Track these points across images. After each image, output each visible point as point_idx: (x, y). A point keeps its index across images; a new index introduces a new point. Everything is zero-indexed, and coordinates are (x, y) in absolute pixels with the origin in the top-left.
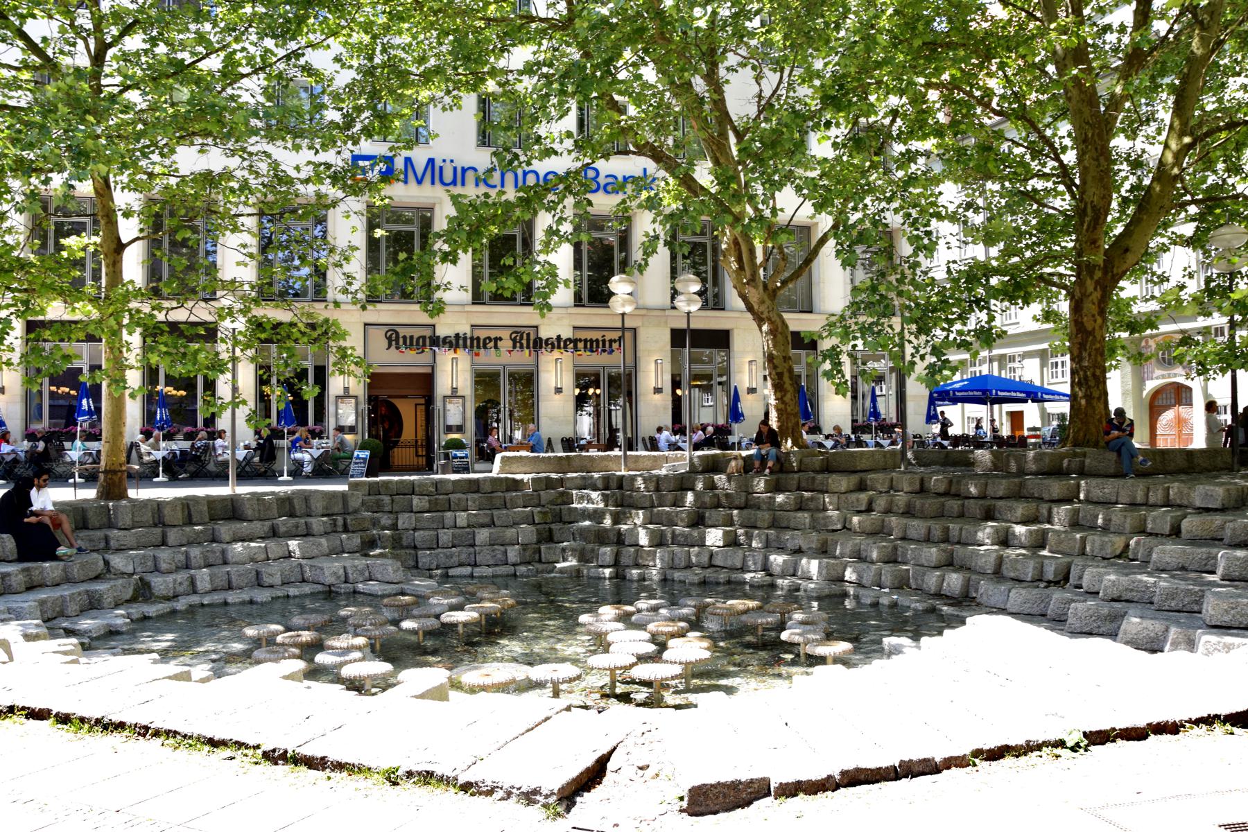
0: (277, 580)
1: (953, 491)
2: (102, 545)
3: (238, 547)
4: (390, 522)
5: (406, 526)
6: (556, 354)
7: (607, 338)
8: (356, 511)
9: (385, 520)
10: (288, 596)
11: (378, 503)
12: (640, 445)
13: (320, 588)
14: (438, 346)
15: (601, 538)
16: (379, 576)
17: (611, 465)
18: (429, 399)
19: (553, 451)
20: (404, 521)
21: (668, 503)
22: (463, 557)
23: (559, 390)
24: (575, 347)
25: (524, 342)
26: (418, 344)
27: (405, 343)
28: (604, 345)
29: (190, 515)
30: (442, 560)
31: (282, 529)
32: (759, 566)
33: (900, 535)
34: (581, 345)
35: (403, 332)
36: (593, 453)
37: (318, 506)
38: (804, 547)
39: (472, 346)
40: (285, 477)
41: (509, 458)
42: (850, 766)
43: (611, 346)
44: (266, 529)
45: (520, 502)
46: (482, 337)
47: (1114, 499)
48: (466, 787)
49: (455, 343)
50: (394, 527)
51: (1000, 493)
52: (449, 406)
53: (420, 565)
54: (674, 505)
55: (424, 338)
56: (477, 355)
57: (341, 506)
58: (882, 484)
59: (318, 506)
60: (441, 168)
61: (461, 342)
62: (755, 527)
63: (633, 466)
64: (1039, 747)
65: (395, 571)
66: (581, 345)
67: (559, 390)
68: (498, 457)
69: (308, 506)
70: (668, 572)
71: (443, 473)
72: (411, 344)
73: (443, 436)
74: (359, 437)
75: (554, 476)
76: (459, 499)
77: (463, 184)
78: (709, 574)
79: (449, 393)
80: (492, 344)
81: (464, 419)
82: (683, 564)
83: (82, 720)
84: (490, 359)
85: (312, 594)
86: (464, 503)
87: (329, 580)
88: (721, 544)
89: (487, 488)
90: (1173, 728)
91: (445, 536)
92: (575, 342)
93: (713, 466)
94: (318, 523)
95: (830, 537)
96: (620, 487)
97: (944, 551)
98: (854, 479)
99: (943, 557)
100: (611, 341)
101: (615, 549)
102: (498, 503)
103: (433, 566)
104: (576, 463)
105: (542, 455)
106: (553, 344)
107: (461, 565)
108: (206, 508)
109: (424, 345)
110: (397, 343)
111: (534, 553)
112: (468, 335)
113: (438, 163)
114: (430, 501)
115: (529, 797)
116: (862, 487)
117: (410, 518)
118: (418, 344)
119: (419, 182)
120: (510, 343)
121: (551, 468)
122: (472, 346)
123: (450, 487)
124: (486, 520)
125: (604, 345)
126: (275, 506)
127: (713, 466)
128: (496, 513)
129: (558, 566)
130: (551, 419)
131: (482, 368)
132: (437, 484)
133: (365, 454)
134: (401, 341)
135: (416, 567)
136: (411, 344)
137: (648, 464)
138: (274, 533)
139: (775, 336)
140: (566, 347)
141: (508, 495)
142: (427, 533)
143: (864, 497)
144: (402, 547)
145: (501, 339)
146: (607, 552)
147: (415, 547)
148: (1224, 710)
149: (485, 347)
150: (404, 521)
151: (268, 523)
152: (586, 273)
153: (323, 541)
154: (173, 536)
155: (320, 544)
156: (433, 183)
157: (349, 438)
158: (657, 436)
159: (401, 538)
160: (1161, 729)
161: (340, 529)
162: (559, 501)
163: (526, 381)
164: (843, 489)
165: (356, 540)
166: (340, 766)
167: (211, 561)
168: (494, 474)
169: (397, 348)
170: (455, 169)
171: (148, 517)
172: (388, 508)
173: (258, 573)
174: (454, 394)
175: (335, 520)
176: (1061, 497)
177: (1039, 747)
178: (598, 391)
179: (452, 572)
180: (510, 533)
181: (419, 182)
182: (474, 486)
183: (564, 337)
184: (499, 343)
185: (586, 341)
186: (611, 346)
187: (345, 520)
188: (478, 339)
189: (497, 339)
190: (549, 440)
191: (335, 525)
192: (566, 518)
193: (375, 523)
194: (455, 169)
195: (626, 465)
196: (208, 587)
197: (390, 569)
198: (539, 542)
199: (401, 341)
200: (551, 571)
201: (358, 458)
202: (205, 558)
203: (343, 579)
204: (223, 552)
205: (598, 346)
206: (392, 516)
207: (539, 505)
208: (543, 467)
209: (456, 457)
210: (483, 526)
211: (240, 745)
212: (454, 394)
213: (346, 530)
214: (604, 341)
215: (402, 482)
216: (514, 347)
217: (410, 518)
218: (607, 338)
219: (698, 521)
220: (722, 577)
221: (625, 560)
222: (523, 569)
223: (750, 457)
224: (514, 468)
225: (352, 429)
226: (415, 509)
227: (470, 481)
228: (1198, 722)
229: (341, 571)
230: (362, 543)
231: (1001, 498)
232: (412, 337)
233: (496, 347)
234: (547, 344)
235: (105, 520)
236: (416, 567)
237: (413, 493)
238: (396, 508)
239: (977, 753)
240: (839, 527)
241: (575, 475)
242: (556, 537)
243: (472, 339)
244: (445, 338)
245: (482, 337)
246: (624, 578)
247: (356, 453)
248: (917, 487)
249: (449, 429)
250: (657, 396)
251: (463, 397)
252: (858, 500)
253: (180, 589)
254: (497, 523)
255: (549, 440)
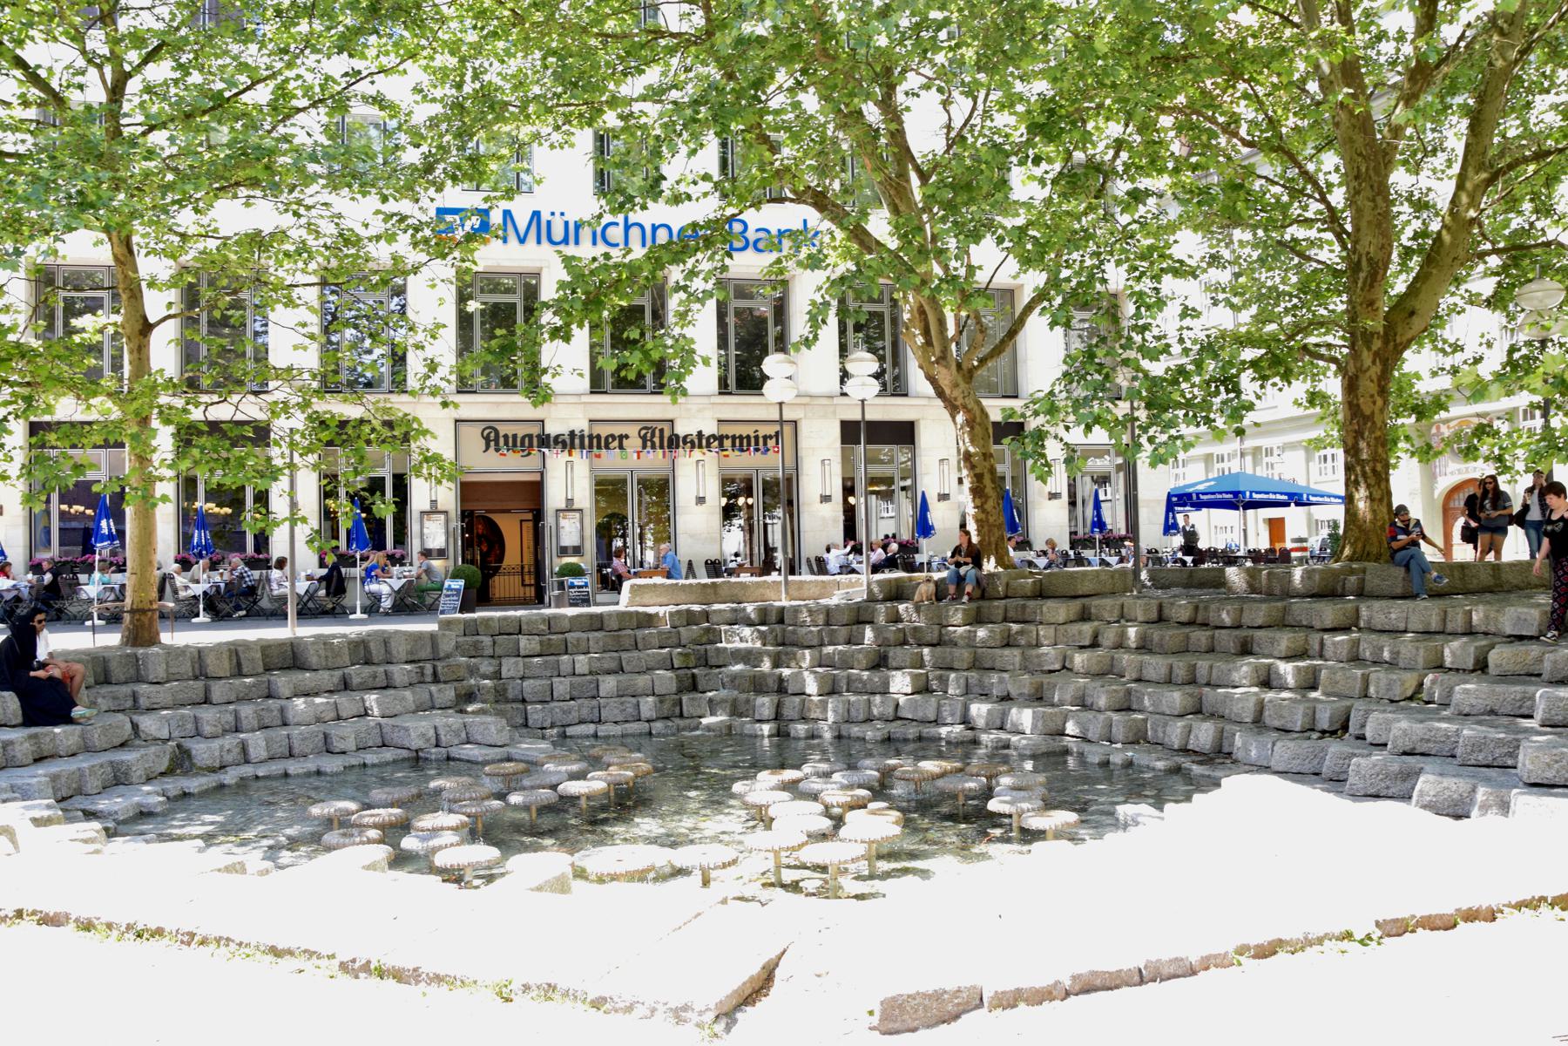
0: (350, 744)
1: (1200, 619)
2: (129, 704)
3: (300, 703)
4: (491, 669)
5: (512, 674)
6: (697, 453)
7: (761, 434)
8: (448, 656)
9: (486, 666)
10: (365, 765)
11: (476, 645)
12: (804, 567)
13: (405, 753)
14: (548, 447)
15: (758, 685)
16: (479, 738)
17: (770, 594)
18: (538, 515)
19: (694, 577)
20: (510, 667)
21: (841, 640)
22: (585, 713)
23: (701, 500)
24: (721, 445)
25: (657, 440)
26: (523, 444)
27: (506, 443)
28: (757, 443)
29: (239, 665)
30: (559, 717)
31: (356, 681)
32: (958, 719)
33: (1134, 676)
34: (727, 443)
35: (503, 429)
36: (745, 578)
37: (400, 650)
38: (1014, 693)
39: (591, 446)
40: (359, 615)
41: (640, 586)
42: (1083, 969)
43: (765, 444)
44: (336, 680)
45: (656, 642)
46: (603, 436)
47: (1402, 626)
48: (597, 1004)
49: (569, 442)
50: (497, 675)
51: (1259, 622)
52: (563, 522)
53: (530, 722)
54: (849, 642)
55: (530, 436)
56: (598, 456)
57: (429, 650)
58: (1111, 612)
59: (400, 650)
60: (549, 223)
61: (577, 441)
62: (952, 669)
63: (795, 593)
64: (1320, 941)
65: (499, 731)
66: (727, 443)
67: (701, 500)
68: (626, 585)
69: (387, 651)
70: (844, 727)
71: (557, 606)
72: (515, 445)
73: (556, 560)
74: (451, 563)
75: (696, 608)
76: (578, 640)
77: (577, 243)
78: (896, 729)
79: (563, 506)
80: (616, 443)
81: (582, 538)
82: (861, 717)
83: (109, 926)
84: (614, 462)
85: (394, 761)
86: (584, 644)
87: (416, 743)
88: (909, 690)
89: (614, 625)
90: (1491, 916)
91: (562, 686)
92: (721, 439)
93: (897, 593)
94: (401, 672)
95: (1046, 679)
96: (781, 621)
97: (1191, 695)
98: (1075, 606)
99: (1190, 703)
100: (765, 438)
101: (775, 698)
102: (628, 643)
103: (547, 724)
104: (724, 592)
105: (682, 582)
106: (692, 442)
107: (581, 722)
108: (259, 655)
109: (531, 445)
110: (497, 444)
111: (674, 705)
112: (586, 433)
113: (545, 217)
114: (541, 643)
115: (679, 1014)
116: (1084, 617)
117: (516, 663)
118: (523, 444)
119: (522, 241)
120: (640, 442)
121: (693, 598)
122: (591, 446)
123: (566, 625)
124: (613, 665)
125: (757, 443)
126: (346, 651)
127: (897, 593)
128: (624, 655)
129: (705, 721)
130: (691, 536)
131: (603, 474)
132: (549, 621)
133: (459, 584)
134: (502, 441)
135: (526, 725)
136: (515, 445)
137: (815, 591)
138: (346, 685)
139: (972, 428)
140: (709, 445)
141: (640, 633)
142: (538, 682)
143: (1087, 628)
144: (507, 701)
145: (627, 437)
146: (765, 704)
147: (524, 701)
148: (1551, 893)
149: (607, 447)
150: (510, 667)
151: (338, 673)
152: (733, 352)
153: (408, 694)
154: (218, 691)
155: (404, 698)
156: (539, 242)
157: (437, 564)
158: (825, 556)
159: (505, 690)
160: (1471, 916)
161: (429, 679)
162: (704, 639)
163: (660, 490)
164: (1061, 620)
165: (448, 693)
166: (438, 979)
167: (267, 721)
168: (621, 607)
169: (497, 450)
170: (566, 223)
171: (186, 668)
172: (489, 652)
173: (326, 737)
174: (570, 507)
175: (422, 668)
176: (1335, 625)
177: (1320, 941)
178: (750, 501)
179: (570, 731)
180: (642, 681)
181: (522, 241)
182: (597, 623)
183: (706, 433)
184: (625, 442)
185: (734, 437)
186: (765, 444)
187: (435, 668)
188: (599, 437)
189: (622, 437)
190: (690, 563)
191: (423, 674)
192: (712, 661)
193: (473, 671)
194: (566, 223)
195: (787, 593)
196: (264, 754)
197: (493, 728)
198: (680, 691)
199: (502, 441)
200: (696, 728)
201: (449, 589)
202: (260, 718)
203: (433, 741)
204: (282, 710)
205: (749, 444)
206: (494, 662)
207: (679, 645)
208: (683, 597)
209: (572, 586)
210: (609, 673)
211: (310, 954)
212: (570, 507)
213: (436, 679)
214: (757, 438)
215: (505, 619)
216: (644, 447)
217: (516, 663)
218: (761, 434)
219: (880, 662)
220: (912, 731)
221: (788, 712)
222: (658, 726)
223: (942, 580)
224: (647, 599)
225: (441, 553)
226: (522, 652)
227: (592, 616)
228: (1519, 906)
229: (431, 733)
230: (458, 696)
231: (1260, 627)
232: (515, 436)
233: (621, 447)
234: (685, 442)
235: (132, 671)
236: (526, 725)
237: (520, 633)
238: (499, 651)
239: (1241, 950)
240: (1057, 666)
241: (722, 606)
242: (701, 684)
243: (591, 437)
244: (557, 437)
245: (603, 436)
246: (788, 735)
247: (447, 584)
248: (1154, 615)
249: (564, 551)
250: (826, 506)
251: (580, 510)
252: (1080, 632)
253: (229, 758)
254: (626, 668)
255: (690, 563)
